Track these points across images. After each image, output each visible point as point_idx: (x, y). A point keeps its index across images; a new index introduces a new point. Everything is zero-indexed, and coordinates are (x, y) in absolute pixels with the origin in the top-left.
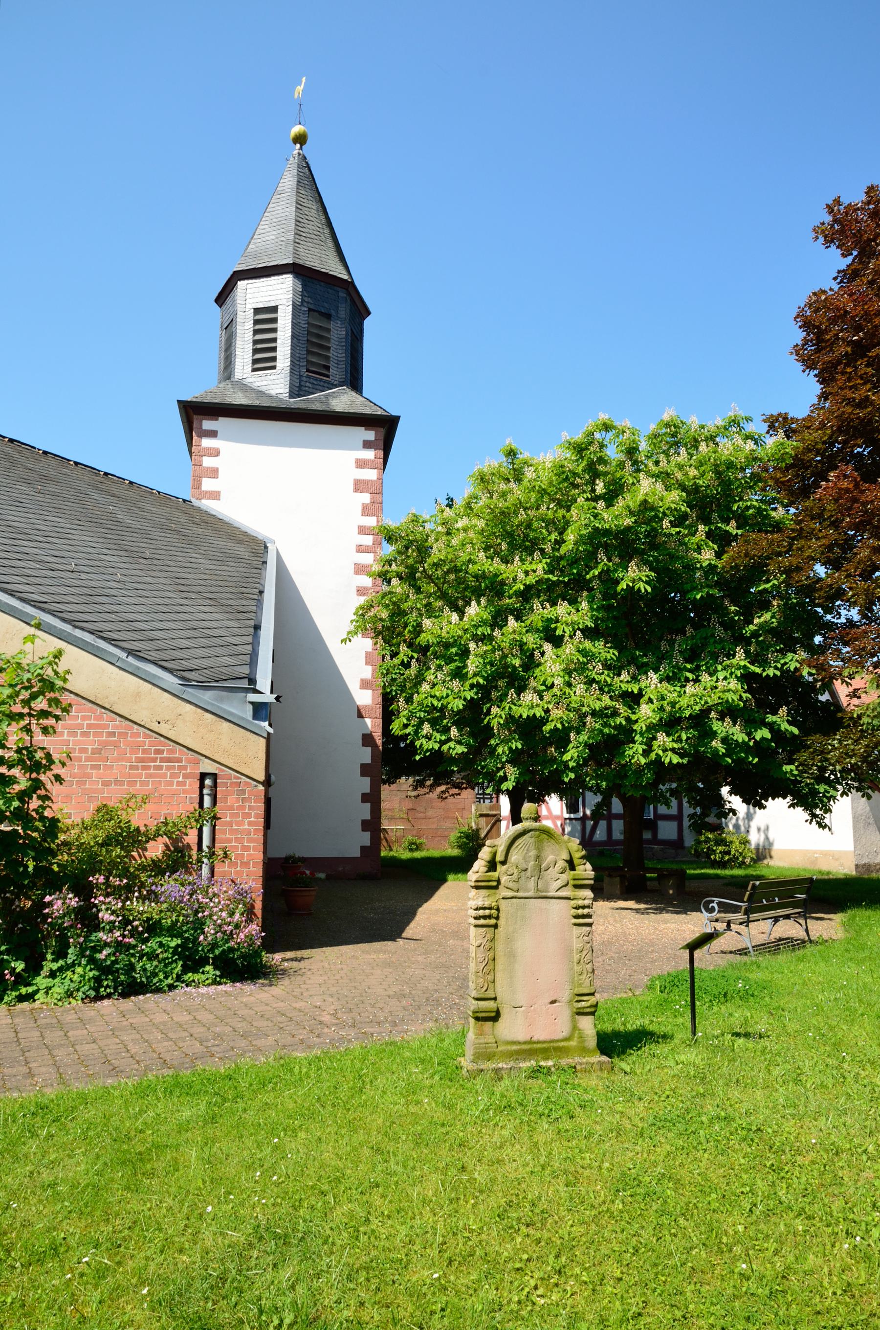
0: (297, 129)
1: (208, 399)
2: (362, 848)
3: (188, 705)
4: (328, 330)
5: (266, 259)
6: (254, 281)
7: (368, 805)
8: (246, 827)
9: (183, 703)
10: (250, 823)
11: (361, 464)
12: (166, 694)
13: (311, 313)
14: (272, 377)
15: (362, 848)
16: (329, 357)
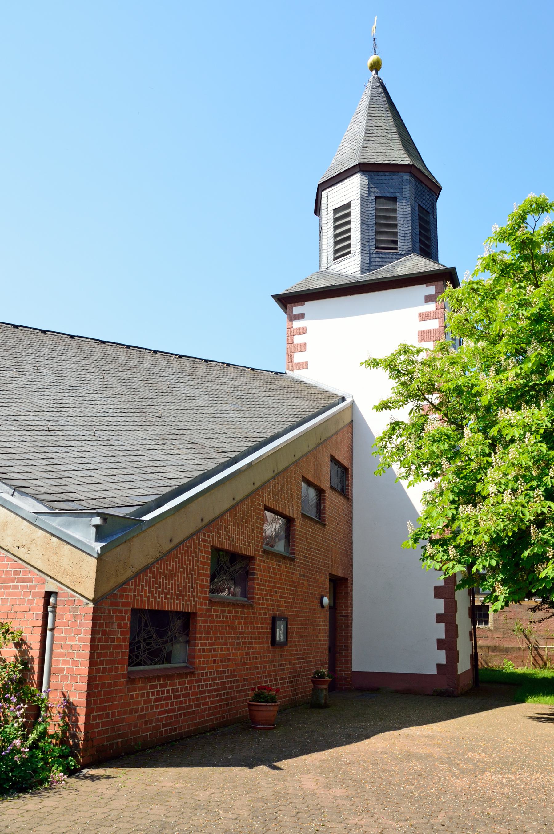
0: (373, 58)
1: (297, 290)
2: (439, 666)
3: (40, 531)
4: (395, 211)
5: (341, 167)
6: (333, 188)
7: (443, 625)
8: (77, 643)
9: (37, 529)
10: (80, 640)
11: (424, 317)
12: (25, 522)
13: (378, 200)
14: (349, 260)
15: (439, 666)
16: (397, 232)
